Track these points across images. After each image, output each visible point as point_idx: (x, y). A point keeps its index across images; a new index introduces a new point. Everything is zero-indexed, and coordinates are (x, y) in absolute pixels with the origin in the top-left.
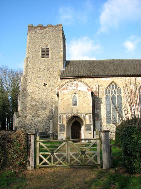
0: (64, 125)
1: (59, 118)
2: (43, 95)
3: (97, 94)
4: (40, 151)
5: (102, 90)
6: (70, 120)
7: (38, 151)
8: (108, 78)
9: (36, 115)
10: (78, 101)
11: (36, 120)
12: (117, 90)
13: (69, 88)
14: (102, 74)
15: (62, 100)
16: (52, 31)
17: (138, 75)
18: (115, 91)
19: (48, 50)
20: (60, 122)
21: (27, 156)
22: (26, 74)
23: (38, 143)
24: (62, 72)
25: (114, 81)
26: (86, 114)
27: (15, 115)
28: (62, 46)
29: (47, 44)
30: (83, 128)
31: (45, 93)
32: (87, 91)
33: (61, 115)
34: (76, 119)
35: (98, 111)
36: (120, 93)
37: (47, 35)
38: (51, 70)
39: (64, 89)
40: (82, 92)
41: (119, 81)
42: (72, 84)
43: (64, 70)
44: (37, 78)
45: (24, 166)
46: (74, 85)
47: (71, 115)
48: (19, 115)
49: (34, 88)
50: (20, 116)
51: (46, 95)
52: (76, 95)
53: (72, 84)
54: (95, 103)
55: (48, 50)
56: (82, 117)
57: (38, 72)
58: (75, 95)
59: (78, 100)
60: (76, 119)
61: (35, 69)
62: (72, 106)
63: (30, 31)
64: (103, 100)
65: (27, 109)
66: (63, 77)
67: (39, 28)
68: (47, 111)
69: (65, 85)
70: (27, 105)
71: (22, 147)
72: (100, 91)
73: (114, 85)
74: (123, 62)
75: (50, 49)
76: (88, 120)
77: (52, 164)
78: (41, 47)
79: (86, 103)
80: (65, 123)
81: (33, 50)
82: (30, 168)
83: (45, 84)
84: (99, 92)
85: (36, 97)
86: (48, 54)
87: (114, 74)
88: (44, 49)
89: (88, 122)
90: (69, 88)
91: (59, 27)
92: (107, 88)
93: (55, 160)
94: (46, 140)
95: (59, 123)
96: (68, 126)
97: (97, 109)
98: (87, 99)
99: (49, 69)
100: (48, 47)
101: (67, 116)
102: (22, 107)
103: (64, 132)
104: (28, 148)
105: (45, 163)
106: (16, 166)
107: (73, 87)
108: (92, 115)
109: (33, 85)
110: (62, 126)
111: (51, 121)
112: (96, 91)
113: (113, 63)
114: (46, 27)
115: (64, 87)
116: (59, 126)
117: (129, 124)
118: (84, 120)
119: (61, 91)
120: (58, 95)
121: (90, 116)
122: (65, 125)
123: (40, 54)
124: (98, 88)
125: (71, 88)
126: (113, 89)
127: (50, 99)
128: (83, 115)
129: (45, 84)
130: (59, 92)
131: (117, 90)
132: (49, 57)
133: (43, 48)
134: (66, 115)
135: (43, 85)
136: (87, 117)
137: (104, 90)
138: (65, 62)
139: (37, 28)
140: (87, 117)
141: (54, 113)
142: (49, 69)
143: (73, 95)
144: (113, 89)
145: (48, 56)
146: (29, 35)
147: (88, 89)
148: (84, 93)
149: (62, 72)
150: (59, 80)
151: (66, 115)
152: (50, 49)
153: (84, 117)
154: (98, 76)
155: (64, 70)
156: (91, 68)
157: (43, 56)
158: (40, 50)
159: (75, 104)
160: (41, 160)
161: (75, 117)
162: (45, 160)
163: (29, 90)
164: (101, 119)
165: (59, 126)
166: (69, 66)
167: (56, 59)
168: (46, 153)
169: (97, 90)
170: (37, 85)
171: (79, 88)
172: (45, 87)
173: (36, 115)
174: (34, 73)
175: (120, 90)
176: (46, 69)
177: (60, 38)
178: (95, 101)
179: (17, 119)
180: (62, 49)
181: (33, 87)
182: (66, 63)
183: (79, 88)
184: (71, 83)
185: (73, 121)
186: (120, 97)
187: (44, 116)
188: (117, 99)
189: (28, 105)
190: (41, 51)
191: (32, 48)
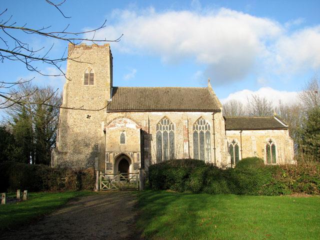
0: (111, 164)
1: (106, 157)
2: (86, 128)
3: (148, 130)
5: (153, 125)
6: (117, 159)
7: (101, 180)
9: (77, 151)
10: (126, 138)
11: (76, 158)
12: (170, 126)
15: (110, 137)
18: (167, 127)
19: (92, 75)
20: (107, 160)
21: (94, 183)
23: (101, 176)
24: (109, 104)
26: (134, 153)
27: (53, 151)
28: (109, 71)
29: (92, 68)
30: (131, 167)
32: (136, 129)
34: (124, 156)
35: (148, 148)
36: (173, 129)
38: (95, 99)
39: (112, 126)
40: (130, 129)
41: (174, 116)
42: (120, 121)
43: (111, 100)
45: (92, 189)
46: (122, 122)
48: (58, 152)
49: (76, 120)
50: (59, 153)
51: (89, 129)
52: (124, 133)
53: (120, 121)
54: (145, 140)
55: (92, 75)
56: (130, 156)
59: (126, 138)
60: (124, 157)
62: (120, 144)
64: (154, 137)
65: (67, 144)
66: (111, 109)
67: (82, 48)
70: (68, 141)
71: (92, 178)
72: (150, 127)
73: (167, 120)
74: (180, 91)
75: (95, 74)
76: (136, 159)
77: (110, 188)
78: (84, 71)
79: (135, 140)
80: (112, 161)
82: (96, 190)
84: (149, 128)
86: (92, 80)
87: (167, 108)
88: (88, 74)
89: (136, 161)
91: (106, 47)
94: (38, 200)
95: (106, 162)
96: (115, 164)
97: (146, 147)
98: (135, 137)
101: (114, 154)
102: (61, 142)
103: (111, 171)
104: (95, 178)
105: (105, 188)
106: (88, 189)
108: (140, 153)
109: (75, 117)
110: (109, 164)
111: (96, 159)
112: (146, 127)
113: (168, 92)
116: (106, 164)
117: (48, 156)
118: (132, 159)
120: (105, 132)
121: (138, 154)
123: (83, 79)
124: (149, 123)
125: (119, 125)
128: (131, 153)
130: (107, 129)
132: (93, 84)
133: (87, 72)
134: (113, 153)
136: (135, 155)
137: (156, 126)
138: (112, 89)
140: (135, 155)
141: (99, 150)
143: (121, 133)
147: (137, 127)
148: (132, 130)
149: (109, 104)
150: (106, 113)
151: (113, 153)
153: (132, 156)
154: (148, 110)
155: (111, 100)
156: (142, 99)
157: (86, 83)
158: (83, 75)
159: (123, 141)
160: (103, 186)
161: (123, 155)
162: (105, 186)
164: (151, 157)
165: (106, 164)
166: (116, 95)
169: (148, 126)
170: (79, 117)
171: (127, 126)
173: (77, 151)
175: (173, 126)
177: (107, 62)
178: (145, 137)
179: (57, 156)
180: (109, 76)
182: (113, 90)
183: (127, 126)
184: (120, 119)
185: (121, 158)
186: (172, 135)
189: (69, 140)
190: (84, 77)
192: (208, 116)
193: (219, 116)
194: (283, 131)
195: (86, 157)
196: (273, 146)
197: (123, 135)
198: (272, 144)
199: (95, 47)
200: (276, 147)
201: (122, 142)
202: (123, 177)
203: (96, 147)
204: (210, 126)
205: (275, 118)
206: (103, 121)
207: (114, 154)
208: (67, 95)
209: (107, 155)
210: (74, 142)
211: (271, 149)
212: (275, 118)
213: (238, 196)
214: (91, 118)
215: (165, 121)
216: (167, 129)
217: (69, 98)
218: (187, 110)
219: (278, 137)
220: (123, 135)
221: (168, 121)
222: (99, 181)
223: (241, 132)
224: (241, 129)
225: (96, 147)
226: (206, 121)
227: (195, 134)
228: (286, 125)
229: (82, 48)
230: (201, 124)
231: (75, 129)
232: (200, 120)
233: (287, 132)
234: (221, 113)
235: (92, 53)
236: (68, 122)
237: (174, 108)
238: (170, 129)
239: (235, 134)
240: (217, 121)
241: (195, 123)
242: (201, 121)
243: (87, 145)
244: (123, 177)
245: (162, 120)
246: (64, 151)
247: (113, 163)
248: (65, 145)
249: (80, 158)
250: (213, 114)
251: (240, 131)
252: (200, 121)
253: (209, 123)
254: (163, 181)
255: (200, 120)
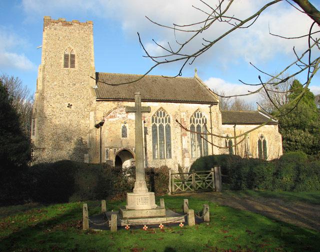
4: (175, 182)
8: (155, 103)
12: (166, 119)
13: (118, 116)
14: (148, 97)
16: (79, 30)
17: (190, 101)
18: (163, 119)
22: (43, 89)
25: (163, 107)
29: (73, 48)
31: (69, 117)
33: (108, 149)
36: (169, 122)
37: (72, 35)
38: (78, 85)
39: (111, 117)
41: (171, 108)
44: (58, 97)
47: (120, 149)
55: (73, 56)
57: (60, 88)
58: (124, 125)
61: (55, 83)
62: (122, 138)
63: (47, 26)
67: (60, 23)
68: (72, 141)
69: (113, 112)
73: (162, 112)
77: (184, 190)
81: (53, 55)
83: (69, 104)
85: (58, 123)
86: (73, 62)
90: (118, 116)
91: (89, 25)
92: (154, 115)
93: (185, 187)
99: (75, 84)
100: (74, 53)
101: (115, 150)
107: (122, 115)
109: (53, 106)
114: (70, 23)
115: (111, 114)
119: (108, 119)
122: (112, 161)
123: (62, 61)
126: (161, 116)
127: (76, 126)
129: (69, 104)
130: (106, 120)
131: (166, 119)
133: (66, 53)
135: (66, 106)
139: (57, 23)
142: (75, 84)
143: (123, 125)
144: (161, 116)
145: (73, 66)
146: (46, 31)
152: (76, 56)
155: (96, 87)
157: (66, 66)
158: (63, 56)
163: (48, 111)
167: (85, 71)
168: (180, 183)
170: (59, 105)
172: (70, 109)
173: (57, 147)
174: (53, 88)
175: (169, 118)
176: (71, 84)
181: (53, 108)
184: (120, 109)
186: (168, 127)
187: (69, 148)
188: (264, 115)
189: (47, 132)
190: (63, 58)
191: (51, 52)
192: (205, 108)
193: (215, 108)
194: (273, 126)
195: (68, 153)
196: (265, 142)
197: (124, 127)
198: (263, 139)
199: (75, 24)
200: (267, 143)
201: (123, 136)
202: (198, 176)
203: (80, 142)
204: (207, 120)
205: (260, 113)
206: (92, 111)
207: (115, 150)
208: (44, 79)
209: (107, 150)
210: (53, 136)
211: (262, 145)
212: (260, 113)
213: (234, 191)
214: (72, 107)
215: (161, 113)
216: (163, 122)
217: (45, 83)
218: (192, 101)
219: (269, 133)
220: (124, 127)
221: (164, 113)
222: (171, 182)
223: (234, 127)
224: (235, 124)
225: (80, 142)
226: (203, 114)
227: (154, 127)
228: (276, 120)
229: (60, 23)
230: (198, 117)
231: (53, 121)
232: (197, 113)
233: (277, 127)
234: (218, 105)
235: (73, 31)
236: (45, 111)
237: (170, 98)
238: (166, 122)
239: (228, 129)
240: (214, 114)
241: (192, 116)
242: (161, 112)
243: (68, 139)
244: (198, 176)
245: (157, 112)
246: (43, 146)
247: (114, 161)
248: (42, 139)
249: (66, 152)
250: (210, 107)
251: (234, 125)
252: (197, 114)
253: (206, 116)
254: (253, 180)
255: (197, 113)
